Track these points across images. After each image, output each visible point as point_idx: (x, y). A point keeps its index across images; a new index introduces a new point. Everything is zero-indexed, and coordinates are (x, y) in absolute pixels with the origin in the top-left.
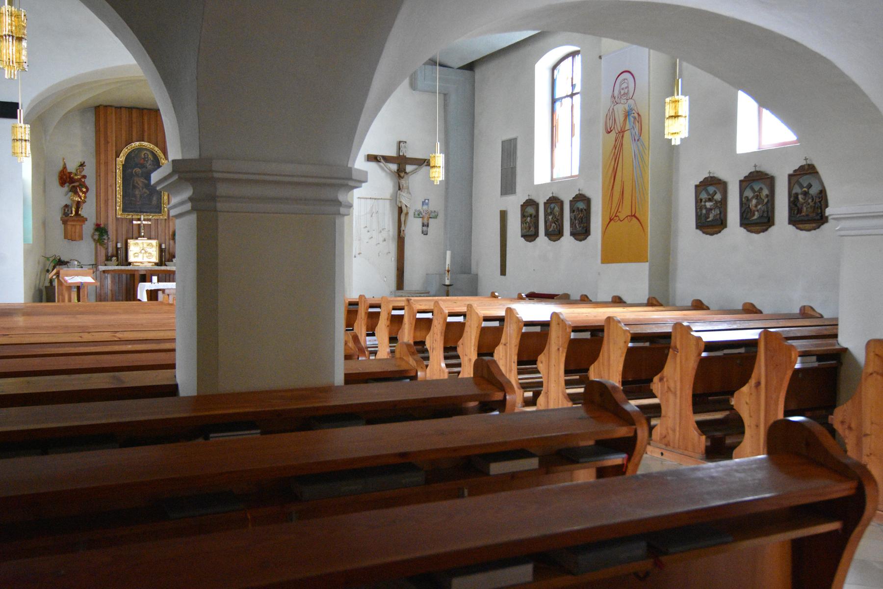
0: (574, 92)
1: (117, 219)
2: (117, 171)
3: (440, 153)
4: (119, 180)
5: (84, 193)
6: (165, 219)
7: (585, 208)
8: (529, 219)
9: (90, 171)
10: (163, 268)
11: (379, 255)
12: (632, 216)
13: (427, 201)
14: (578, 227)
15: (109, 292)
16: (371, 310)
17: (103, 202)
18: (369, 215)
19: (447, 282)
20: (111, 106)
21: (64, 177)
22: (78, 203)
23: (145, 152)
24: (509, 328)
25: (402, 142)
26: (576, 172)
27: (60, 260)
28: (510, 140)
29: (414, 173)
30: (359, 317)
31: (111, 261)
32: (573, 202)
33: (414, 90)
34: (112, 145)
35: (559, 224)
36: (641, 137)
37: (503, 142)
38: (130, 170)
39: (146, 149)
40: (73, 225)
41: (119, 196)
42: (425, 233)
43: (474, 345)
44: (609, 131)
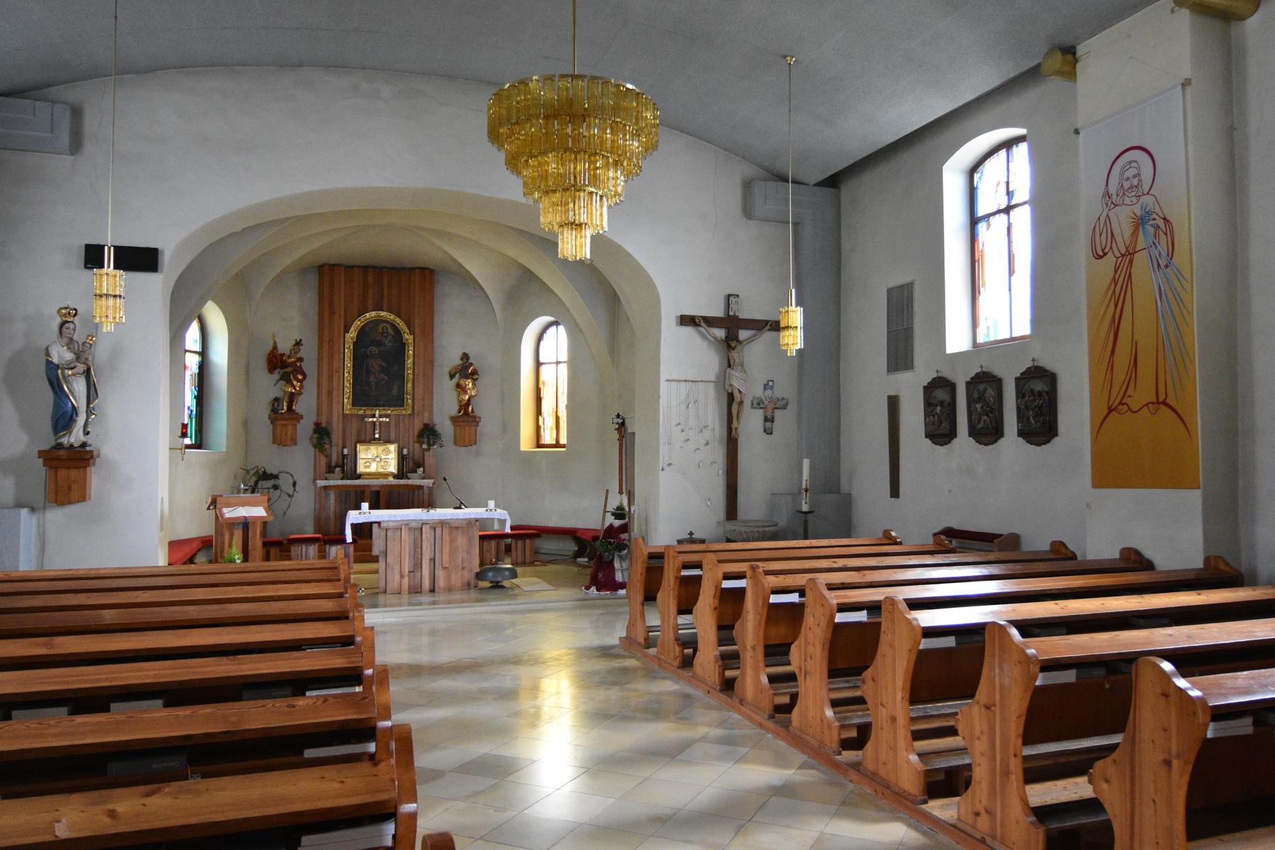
0: (1013, 203)
1: (345, 416)
2: (346, 351)
3: (796, 306)
4: (349, 364)
5: (299, 381)
6: (409, 415)
7: (1046, 390)
8: (939, 408)
9: (309, 353)
10: (403, 482)
11: (699, 467)
12: (1158, 403)
13: (771, 383)
14: (1033, 422)
15: (332, 516)
16: (685, 573)
17: (328, 393)
18: (683, 407)
19: (805, 508)
20: (338, 265)
21: (275, 361)
22: (292, 394)
23: (385, 325)
24: (997, 671)
25: (731, 295)
26: (1023, 328)
27: (265, 473)
28: (902, 287)
29: (750, 342)
30: (665, 583)
31: (334, 473)
32: (1021, 381)
33: (750, 219)
34: (340, 316)
35: (995, 417)
36: (1174, 260)
37: (889, 291)
38: (363, 350)
39: (386, 321)
40: (284, 425)
41: (348, 385)
42: (768, 432)
43: (903, 689)
44: (1101, 254)
